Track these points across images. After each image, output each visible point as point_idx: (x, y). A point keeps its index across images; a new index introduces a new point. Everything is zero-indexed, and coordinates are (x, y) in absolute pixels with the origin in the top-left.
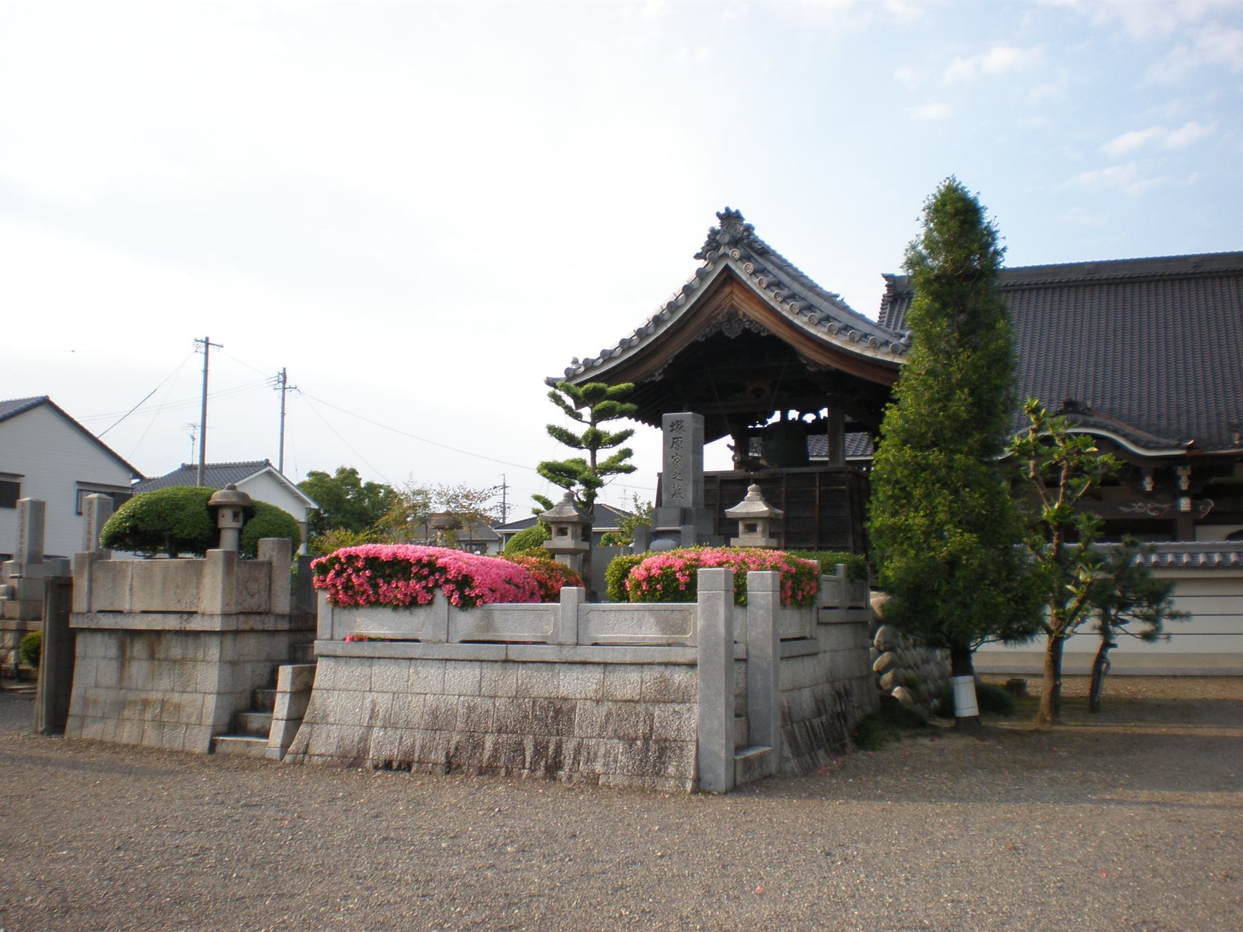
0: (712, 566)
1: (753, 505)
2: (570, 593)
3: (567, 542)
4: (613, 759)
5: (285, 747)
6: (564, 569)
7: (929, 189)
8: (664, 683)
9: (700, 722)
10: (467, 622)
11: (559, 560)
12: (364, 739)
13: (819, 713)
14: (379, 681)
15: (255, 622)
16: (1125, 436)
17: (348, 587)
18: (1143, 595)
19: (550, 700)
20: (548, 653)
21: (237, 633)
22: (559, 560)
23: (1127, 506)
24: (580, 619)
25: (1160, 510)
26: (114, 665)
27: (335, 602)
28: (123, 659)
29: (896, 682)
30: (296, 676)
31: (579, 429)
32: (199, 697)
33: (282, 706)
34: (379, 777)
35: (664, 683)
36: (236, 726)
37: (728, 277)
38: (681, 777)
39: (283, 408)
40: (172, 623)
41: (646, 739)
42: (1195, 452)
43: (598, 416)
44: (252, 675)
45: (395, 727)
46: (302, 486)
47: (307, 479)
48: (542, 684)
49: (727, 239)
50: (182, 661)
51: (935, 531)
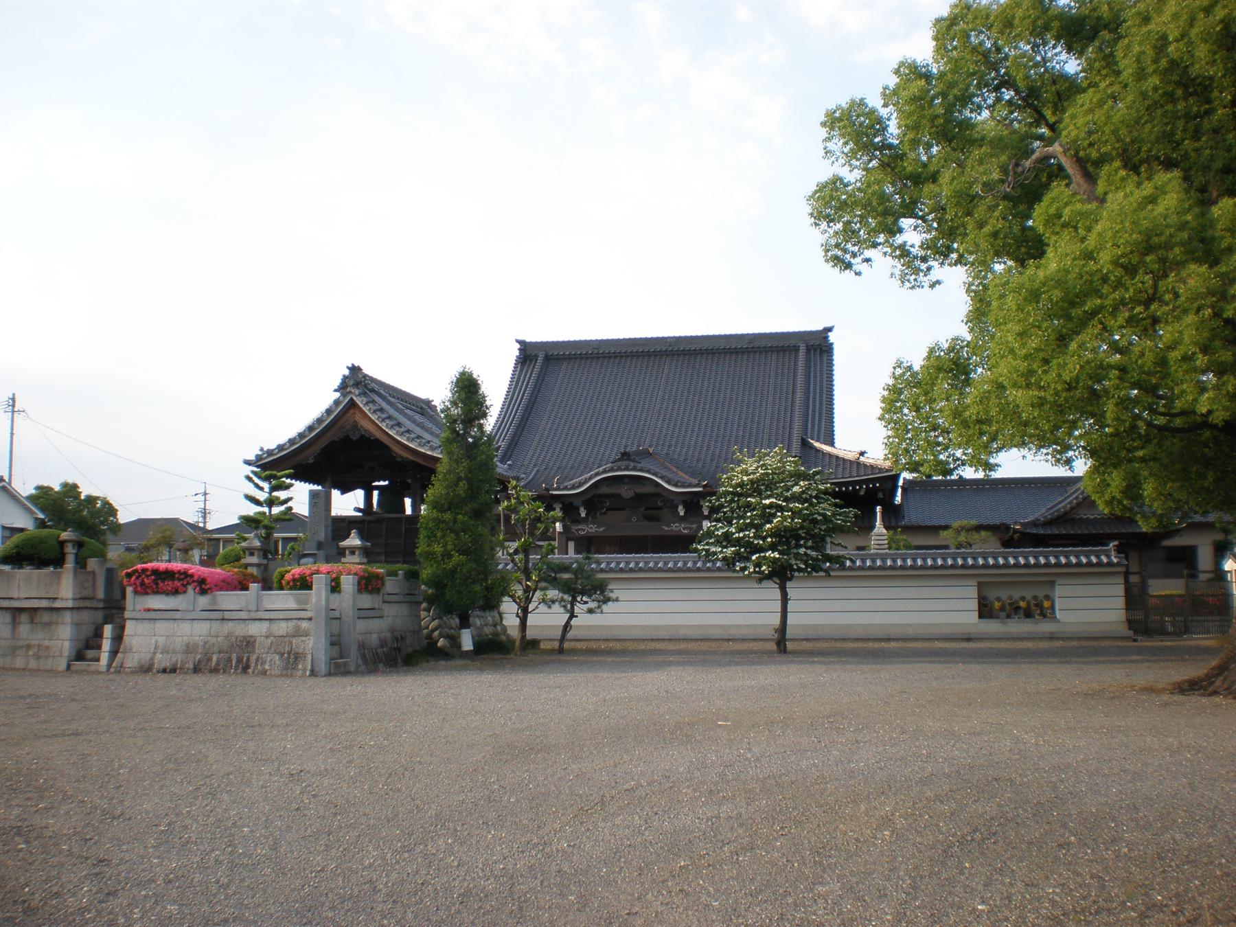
0: (320, 574)
1: (354, 541)
2: (254, 587)
3: (254, 560)
4: (273, 662)
5: (109, 665)
6: (252, 575)
7: (452, 374)
8: (298, 628)
9: (314, 645)
10: (203, 601)
11: (250, 570)
12: (152, 659)
13: (382, 646)
14: (157, 629)
15: (88, 604)
16: (662, 478)
17: (142, 584)
18: (584, 587)
19: (244, 637)
20: (243, 615)
21: (79, 608)
22: (250, 570)
23: (669, 526)
24: (259, 598)
25: (691, 529)
26: (10, 626)
27: (136, 592)
28: (15, 623)
29: (441, 636)
30: (114, 629)
31: (262, 496)
32: (59, 642)
33: (106, 645)
34: (161, 676)
35: (298, 628)
36: (80, 656)
37: (352, 404)
38: (305, 670)
39: (12, 429)
40: (44, 604)
41: (289, 653)
42: (708, 489)
43: (273, 489)
44: (88, 631)
45: (167, 652)
46: (31, 498)
47: (34, 492)
48: (241, 630)
49: (351, 383)
50: (49, 624)
51: (447, 555)
